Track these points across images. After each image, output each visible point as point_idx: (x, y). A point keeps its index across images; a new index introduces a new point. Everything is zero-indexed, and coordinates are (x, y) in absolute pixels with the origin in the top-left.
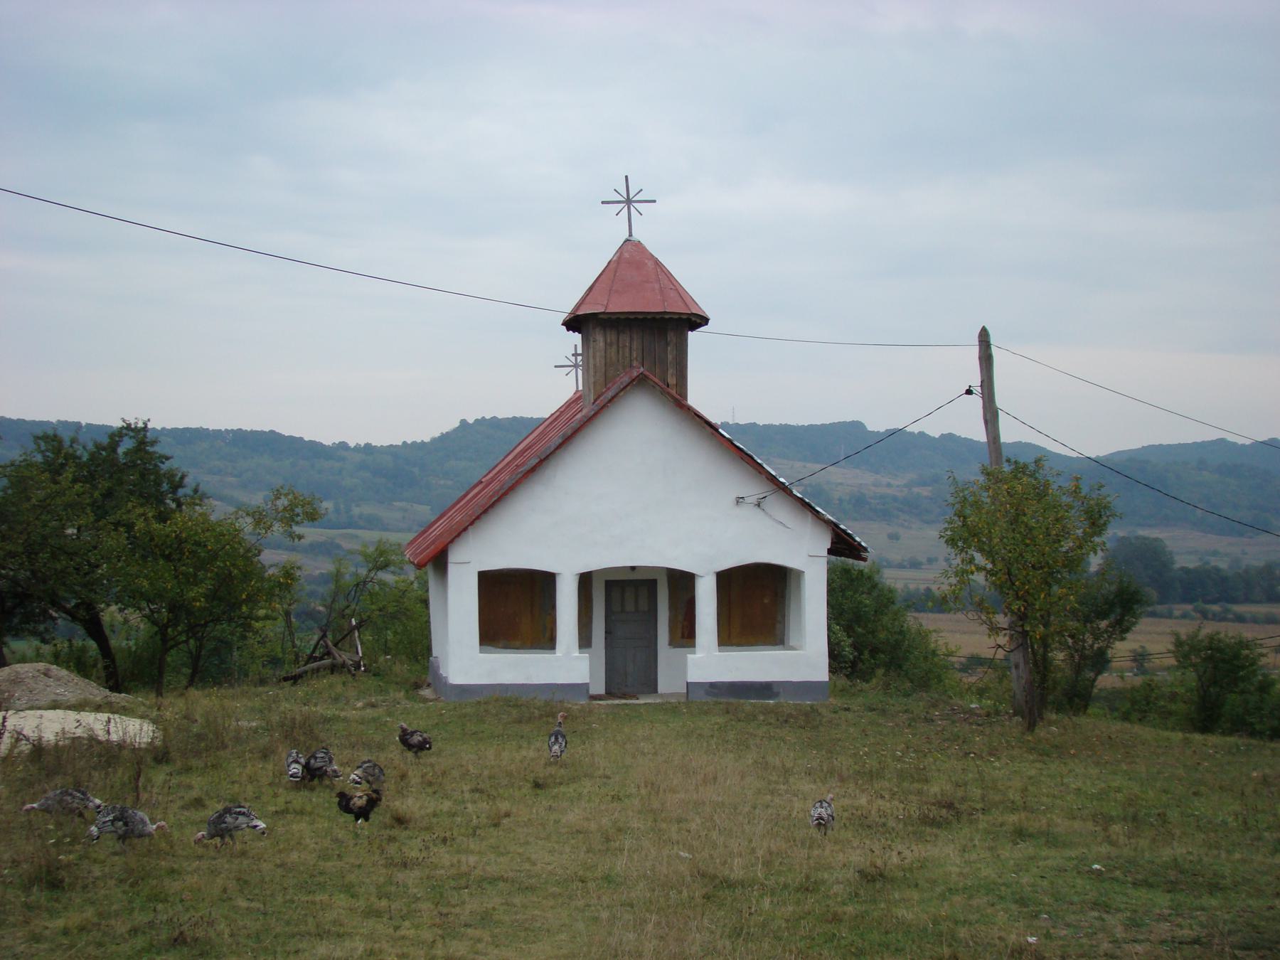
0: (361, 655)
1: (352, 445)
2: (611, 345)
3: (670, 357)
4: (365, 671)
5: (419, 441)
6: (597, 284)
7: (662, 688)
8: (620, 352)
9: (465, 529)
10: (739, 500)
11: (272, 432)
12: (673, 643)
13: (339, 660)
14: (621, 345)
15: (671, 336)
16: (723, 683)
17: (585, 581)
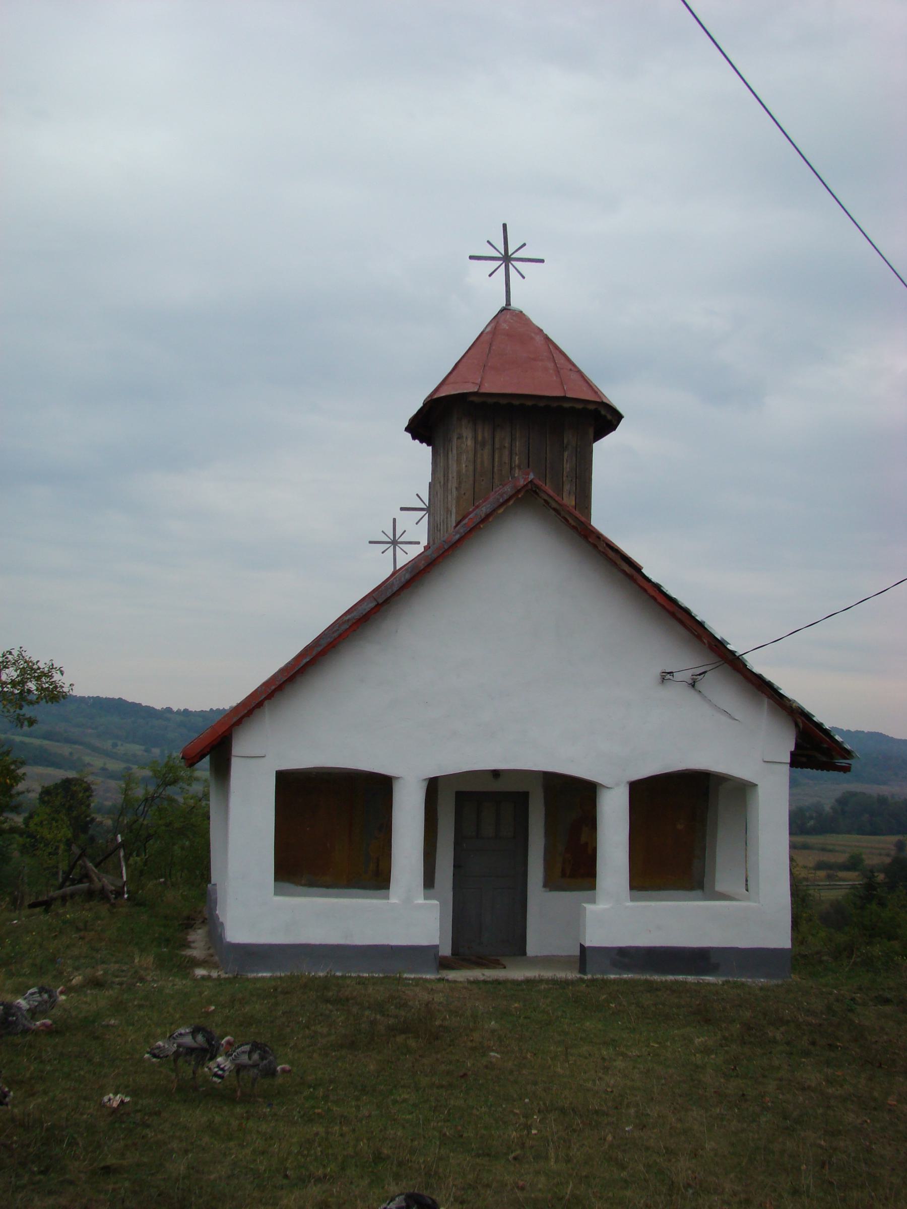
0: (125, 879)
1: (175, 709)
2: (483, 444)
3: (567, 466)
4: (128, 899)
5: (221, 708)
6: (464, 360)
7: (533, 948)
8: (496, 456)
9: (260, 705)
10: (666, 677)
11: (120, 699)
12: (550, 884)
13: (97, 885)
14: (497, 446)
15: (569, 438)
16: (637, 949)
17: (433, 786)
